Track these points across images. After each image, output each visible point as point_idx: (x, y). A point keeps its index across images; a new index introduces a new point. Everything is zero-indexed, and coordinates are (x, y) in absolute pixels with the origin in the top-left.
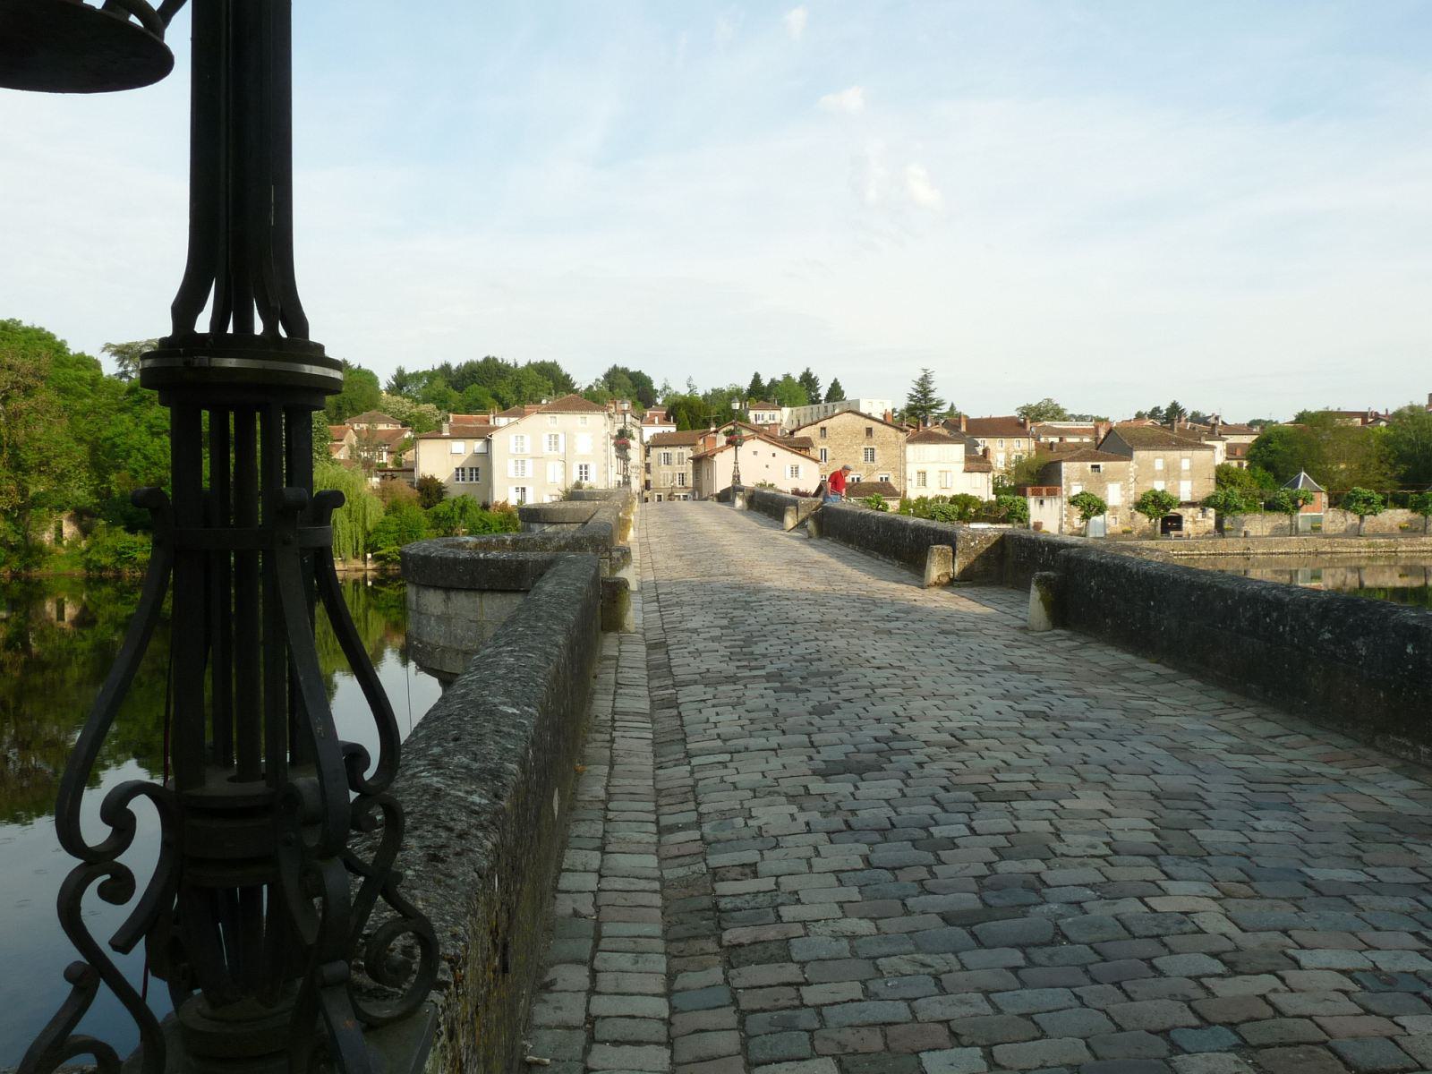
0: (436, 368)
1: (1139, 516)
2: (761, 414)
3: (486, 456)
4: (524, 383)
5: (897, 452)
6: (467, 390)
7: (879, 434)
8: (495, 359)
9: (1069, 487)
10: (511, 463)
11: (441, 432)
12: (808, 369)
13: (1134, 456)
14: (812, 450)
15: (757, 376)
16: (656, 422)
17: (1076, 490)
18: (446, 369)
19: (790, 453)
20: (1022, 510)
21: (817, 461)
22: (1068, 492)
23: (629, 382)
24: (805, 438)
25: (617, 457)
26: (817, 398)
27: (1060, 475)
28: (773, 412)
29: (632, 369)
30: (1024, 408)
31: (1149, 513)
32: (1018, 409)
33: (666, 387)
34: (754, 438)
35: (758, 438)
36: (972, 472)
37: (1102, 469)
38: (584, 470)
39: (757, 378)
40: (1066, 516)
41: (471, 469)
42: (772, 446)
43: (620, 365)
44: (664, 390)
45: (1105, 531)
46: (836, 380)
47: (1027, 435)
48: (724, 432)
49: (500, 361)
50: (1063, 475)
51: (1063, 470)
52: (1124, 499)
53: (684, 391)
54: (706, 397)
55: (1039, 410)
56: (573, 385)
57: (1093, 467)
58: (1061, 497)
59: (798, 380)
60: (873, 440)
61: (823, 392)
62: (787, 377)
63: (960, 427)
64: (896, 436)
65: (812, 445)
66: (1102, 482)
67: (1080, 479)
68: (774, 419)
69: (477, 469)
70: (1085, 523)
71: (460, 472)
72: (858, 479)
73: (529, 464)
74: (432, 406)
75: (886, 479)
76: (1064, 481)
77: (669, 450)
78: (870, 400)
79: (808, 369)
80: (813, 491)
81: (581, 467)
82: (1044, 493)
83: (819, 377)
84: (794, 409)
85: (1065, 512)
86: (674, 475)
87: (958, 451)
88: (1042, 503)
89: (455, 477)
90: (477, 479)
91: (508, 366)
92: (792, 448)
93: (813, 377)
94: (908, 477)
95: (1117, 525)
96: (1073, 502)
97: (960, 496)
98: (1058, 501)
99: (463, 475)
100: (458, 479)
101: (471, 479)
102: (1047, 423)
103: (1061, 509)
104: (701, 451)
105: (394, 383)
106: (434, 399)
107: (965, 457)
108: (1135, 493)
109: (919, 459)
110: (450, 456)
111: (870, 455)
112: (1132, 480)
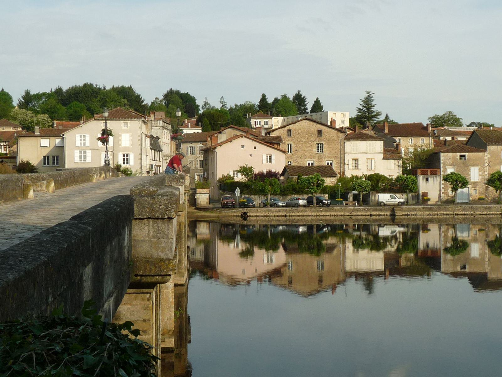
0: (53, 90)
1: (491, 189)
2: (259, 121)
3: (61, 148)
4: (108, 100)
5: (338, 146)
6: (70, 105)
7: (326, 134)
8: (91, 85)
9: (445, 170)
10: (77, 154)
11: (34, 132)
12: (299, 92)
13: (488, 149)
14: (281, 145)
15: (264, 97)
16: (190, 126)
17: (450, 171)
18: (59, 91)
19: (266, 147)
20: (413, 184)
21: (284, 152)
22: (445, 173)
23: (180, 100)
24: (277, 137)
25: (152, 149)
26: (305, 111)
27: (440, 161)
28: (266, 120)
29: (182, 91)
30: (433, 117)
31: (495, 187)
32: (429, 118)
33: (206, 104)
34: (242, 137)
35: (245, 137)
36: (388, 159)
37: (467, 157)
38: (126, 158)
39: (264, 98)
40: (443, 188)
41: (54, 157)
42: (254, 142)
43: (174, 89)
44: (205, 105)
45: (469, 198)
46: (317, 99)
47: (427, 135)
48: (461, 125)
49: (95, 86)
50: (442, 161)
51: (441, 158)
52: (481, 177)
53: (218, 106)
54: (231, 109)
55: (444, 118)
56: (143, 101)
57: (461, 156)
58: (440, 176)
59: (291, 99)
60: (322, 138)
61: (309, 107)
62: (284, 97)
63: (384, 130)
64: (338, 136)
65: (282, 141)
66: (467, 167)
67: (452, 164)
68: (267, 125)
69: (57, 157)
70: (454, 193)
71: (46, 159)
72: (312, 164)
73: (89, 153)
74: (46, 116)
75: (331, 164)
76: (442, 165)
77: (193, 145)
78: (342, 113)
79: (299, 92)
80: (281, 173)
81: (124, 156)
82: (429, 173)
83: (306, 97)
84: (285, 118)
85: (442, 186)
86: (196, 162)
87: (379, 145)
88: (427, 179)
89: (43, 162)
90: (57, 164)
91: (100, 89)
92: (267, 143)
93: (302, 97)
94: (346, 162)
95: (477, 194)
96: (446, 179)
97: (374, 175)
98: (438, 179)
99: (48, 160)
100: (45, 164)
101: (54, 164)
102: (446, 127)
103: (440, 183)
104: (209, 144)
105: (23, 101)
106: (48, 111)
107: (384, 149)
108: (488, 173)
109: (354, 151)
110: (39, 149)
111: (320, 148)
112: (486, 165)
